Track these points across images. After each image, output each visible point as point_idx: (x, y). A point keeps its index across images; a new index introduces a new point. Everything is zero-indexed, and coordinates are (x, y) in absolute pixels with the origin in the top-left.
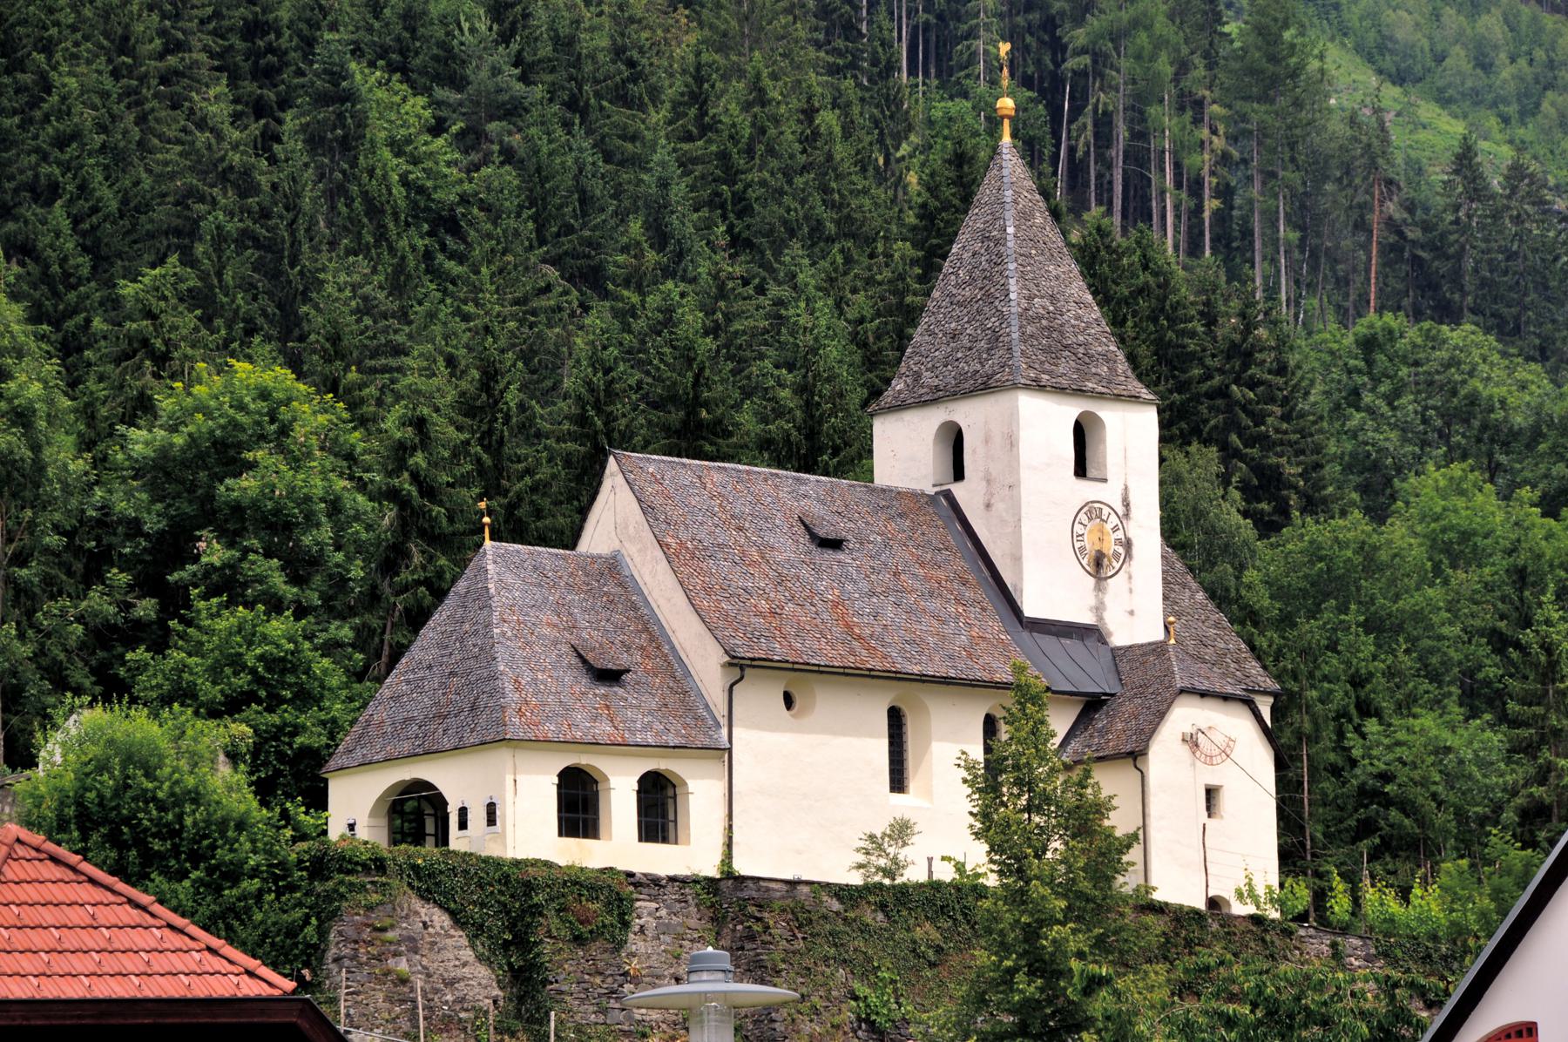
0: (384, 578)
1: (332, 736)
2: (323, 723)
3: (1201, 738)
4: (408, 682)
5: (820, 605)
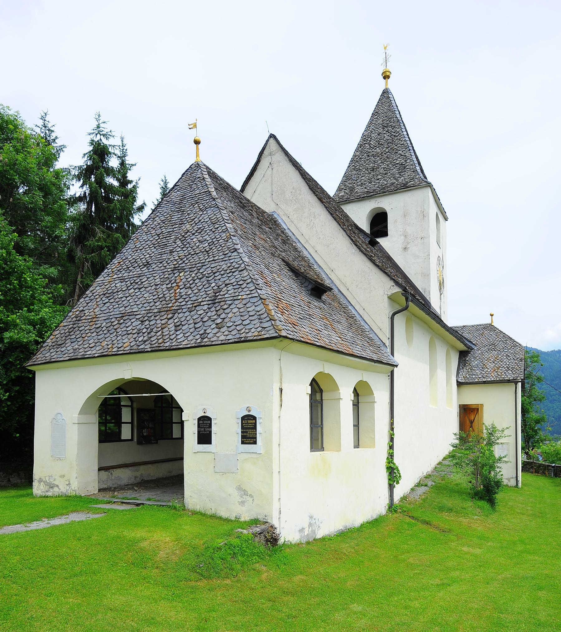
0: (77, 247)
1: (40, 335)
2: (32, 323)
4: (122, 280)
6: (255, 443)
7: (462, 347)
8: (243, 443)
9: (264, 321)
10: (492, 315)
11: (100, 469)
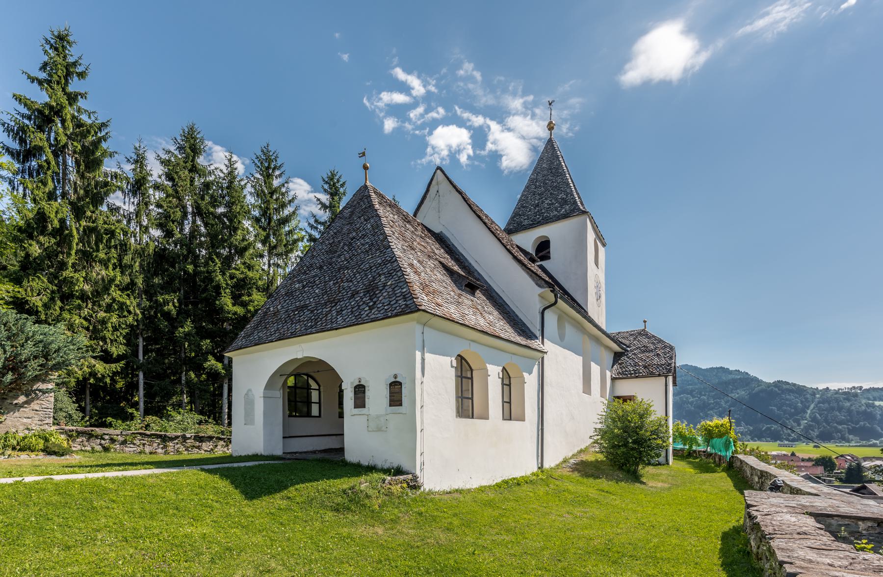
6: (401, 405)
7: (617, 348)
8: (390, 405)
9: (407, 299)
10: (645, 322)
11: (284, 438)
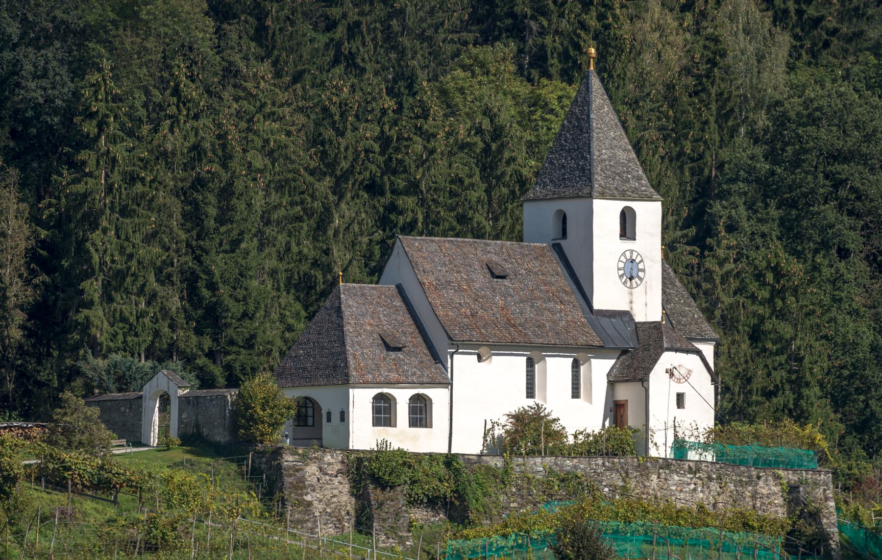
3: (675, 372)
5: (495, 309)
